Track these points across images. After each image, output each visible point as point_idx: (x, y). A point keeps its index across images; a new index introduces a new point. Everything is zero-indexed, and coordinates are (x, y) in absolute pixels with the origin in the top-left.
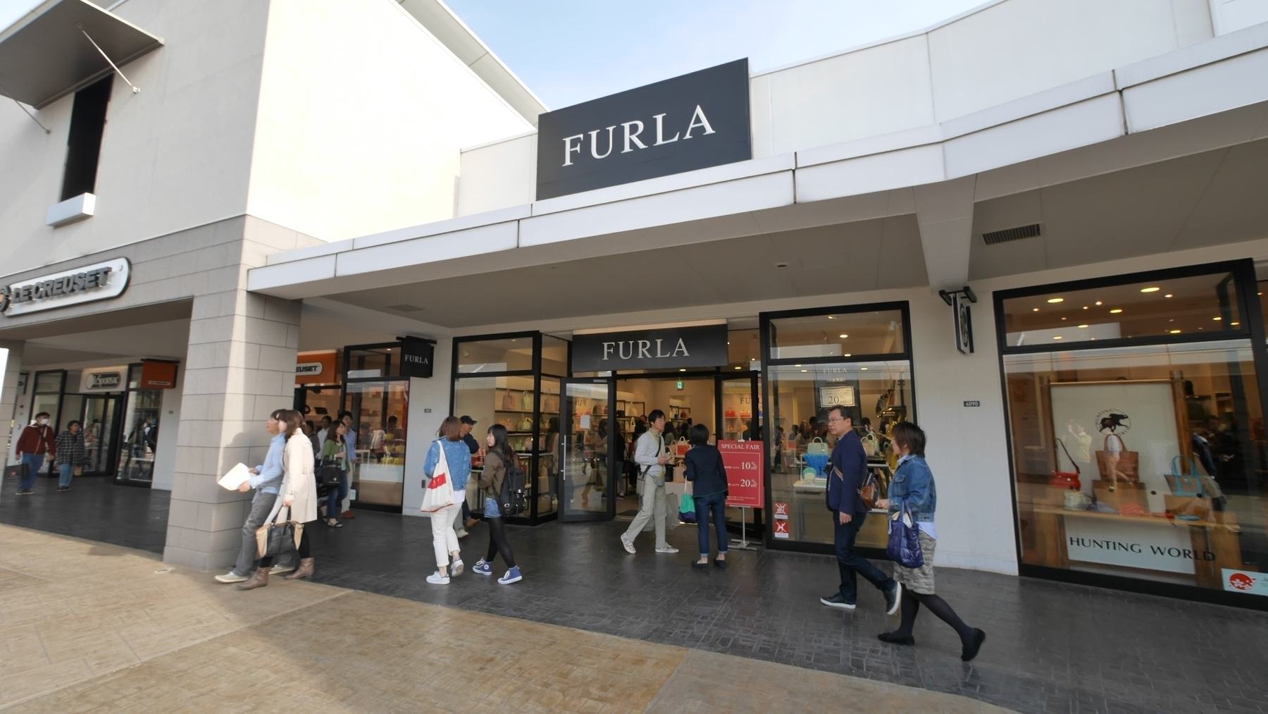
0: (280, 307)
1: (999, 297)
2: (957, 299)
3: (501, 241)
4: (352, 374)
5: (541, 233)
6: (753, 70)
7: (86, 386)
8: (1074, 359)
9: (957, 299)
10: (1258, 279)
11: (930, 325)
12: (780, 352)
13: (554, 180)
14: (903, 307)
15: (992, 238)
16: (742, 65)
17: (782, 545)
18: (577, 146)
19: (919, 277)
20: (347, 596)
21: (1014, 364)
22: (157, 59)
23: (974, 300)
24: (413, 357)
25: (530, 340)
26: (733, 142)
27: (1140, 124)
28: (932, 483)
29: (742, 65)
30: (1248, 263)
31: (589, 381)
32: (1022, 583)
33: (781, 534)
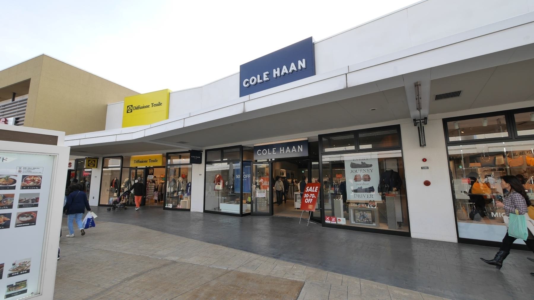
1: (445, 121)
6: (315, 40)
9: (420, 123)
11: (408, 135)
12: (451, 139)
15: (438, 97)
16: (311, 39)
22: (313, 38)
29: (311, 39)
31: (262, 163)
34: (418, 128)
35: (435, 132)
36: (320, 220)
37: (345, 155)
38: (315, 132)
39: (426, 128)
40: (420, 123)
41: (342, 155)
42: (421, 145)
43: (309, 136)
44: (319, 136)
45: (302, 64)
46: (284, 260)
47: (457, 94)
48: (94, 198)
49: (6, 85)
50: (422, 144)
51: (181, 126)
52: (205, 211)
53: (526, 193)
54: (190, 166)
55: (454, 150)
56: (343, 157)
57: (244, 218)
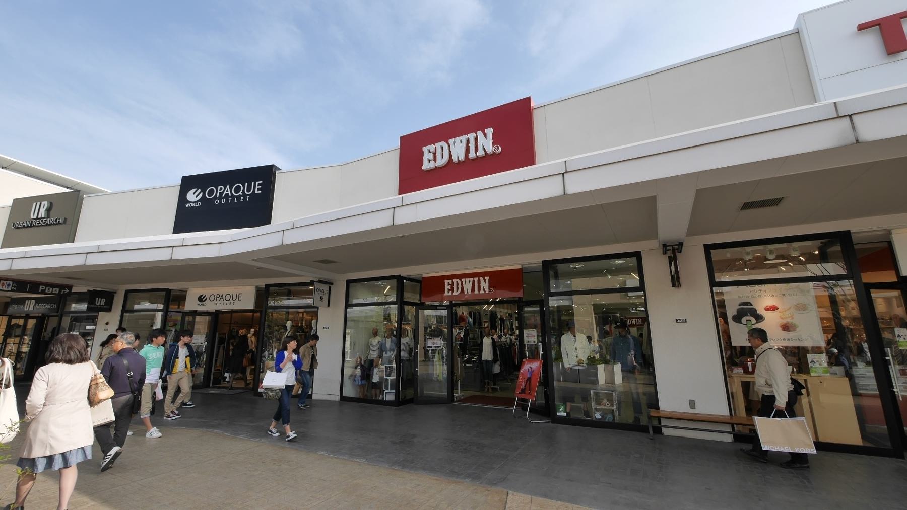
1: (708, 248)
3: (381, 221)
5: (405, 217)
6: (533, 104)
7: (191, 304)
9: (672, 251)
11: (656, 269)
14: (638, 255)
16: (527, 100)
17: (561, 421)
19: (651, 232)
20: (43, 385)
25: (164, 293)
27: (398, 221)
28: (70, 362)
29: (527, 100)
30: (847, 233)
33: (561, 413)
35: (694, 263)
40: (672, 251)
42: (673, 285)
43: (525, 262)
44: (544, 262)
45: (193, 196)
46: (430, 469)
47: (776, 202)
49: (659, 216)
50: (676, 281)
51: (167, 257)
52: (343, 399)
53: (882, 396)
55: (57, 457)
56: (722, 293)
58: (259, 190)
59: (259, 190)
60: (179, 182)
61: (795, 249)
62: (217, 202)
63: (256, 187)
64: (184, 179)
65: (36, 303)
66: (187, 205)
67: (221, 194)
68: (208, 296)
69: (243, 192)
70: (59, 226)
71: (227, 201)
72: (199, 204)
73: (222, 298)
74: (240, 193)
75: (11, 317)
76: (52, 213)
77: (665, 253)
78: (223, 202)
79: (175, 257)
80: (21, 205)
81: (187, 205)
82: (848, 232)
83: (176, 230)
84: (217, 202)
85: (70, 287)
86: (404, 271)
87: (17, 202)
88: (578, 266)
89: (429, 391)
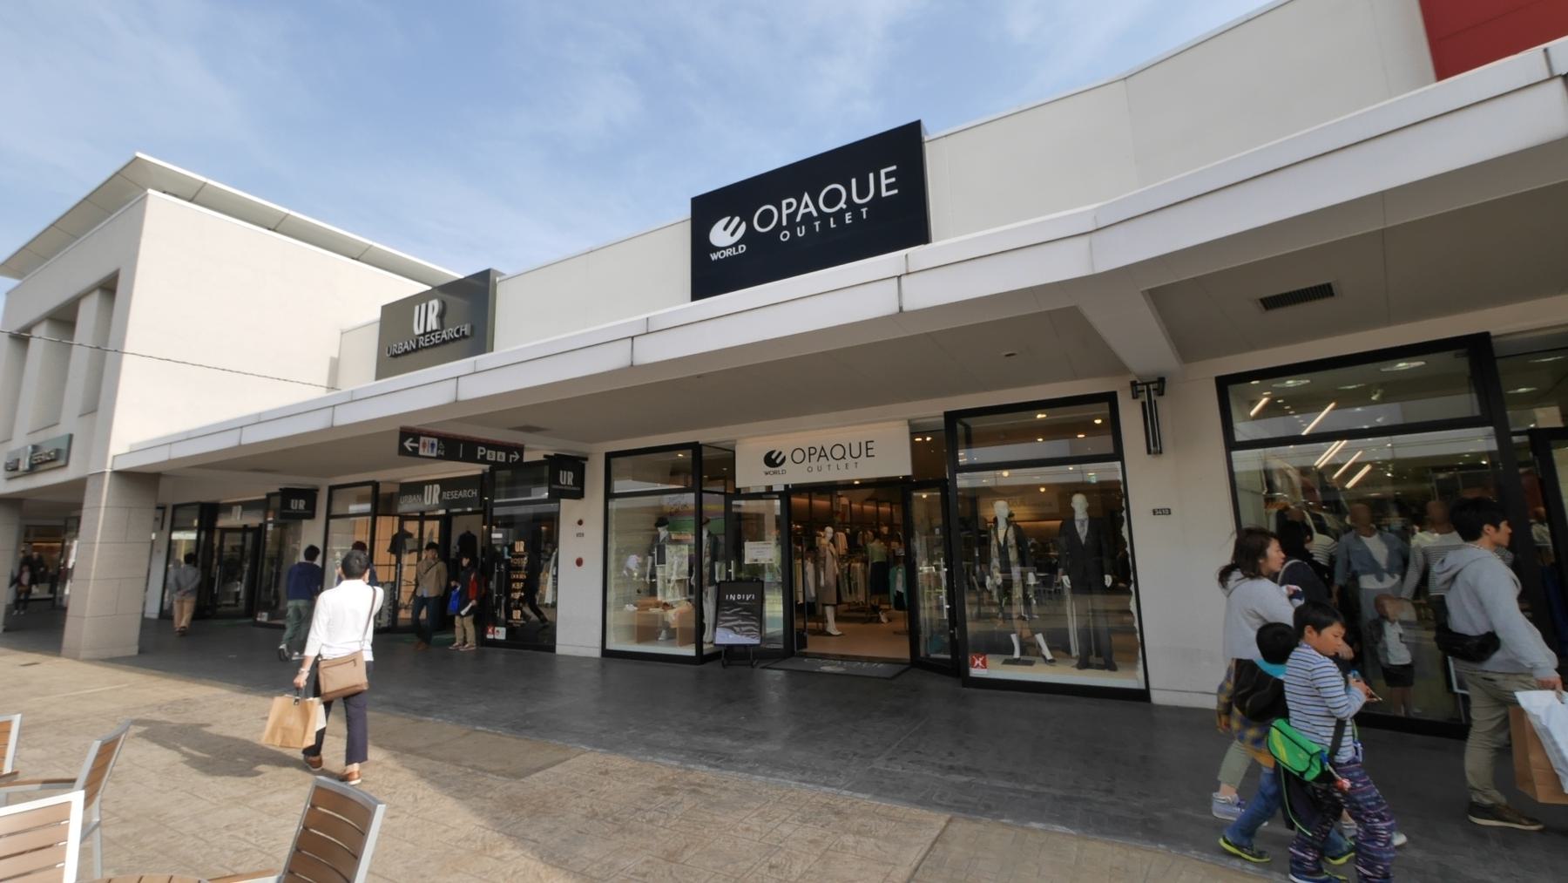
0: (140, 481)
1: (1224, 384)
2: (1151, 389)
4: (964, 457)
6: (929, 133)
8: (1427, 443)
10: (1497, 354)
13: (711, 276)
18: (754, 229)
21: (1247, 461)
22: (926, 125)
23: (1161, 393)
24: (564, 472)
26: (903, 222)
30: (1484, 338)
32: (603, 666)
34: (1143, 404)
36: (956, 669)
37: (666, 497)
38: (936, 401)
39: (1164, 405)
40: (1151, 389)
41: (1085, 466)
42: (1149, 452)
45: (723, 235)
47: (1325, 291)
48: (579, 562)
52: (606, 653)
54: (552, 507)
57: (708, 667)
58: (889, 187)
59: (889, 187)
60: (686, 212)
61: (1349, 379)
62: (785, 236)
63: (884, 183)
64: (696, 202)
65: (442, 490)
66: (714, 257)
67: (791, 217)
68: (787, 453)
69: (849, 200)
70: (464, 342)
71: (810, 228)
72: (743, 248)
73: (823, 454)
74: (842, 205)
75: (404, 518)
76: (446, 319)
77: (1135, 397)
78: (801, 232)
79: (339, 422)
80: (396, 315)
81: (714, 257)
82: (1487, 334)
83: (1444, 69)
84: (785, 236)
85: (520, 449)
86: (1502, 320)
87: (386, 309)
88: (1290, 383)
89: (485, 632)
